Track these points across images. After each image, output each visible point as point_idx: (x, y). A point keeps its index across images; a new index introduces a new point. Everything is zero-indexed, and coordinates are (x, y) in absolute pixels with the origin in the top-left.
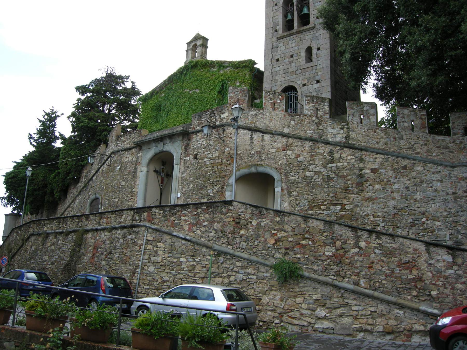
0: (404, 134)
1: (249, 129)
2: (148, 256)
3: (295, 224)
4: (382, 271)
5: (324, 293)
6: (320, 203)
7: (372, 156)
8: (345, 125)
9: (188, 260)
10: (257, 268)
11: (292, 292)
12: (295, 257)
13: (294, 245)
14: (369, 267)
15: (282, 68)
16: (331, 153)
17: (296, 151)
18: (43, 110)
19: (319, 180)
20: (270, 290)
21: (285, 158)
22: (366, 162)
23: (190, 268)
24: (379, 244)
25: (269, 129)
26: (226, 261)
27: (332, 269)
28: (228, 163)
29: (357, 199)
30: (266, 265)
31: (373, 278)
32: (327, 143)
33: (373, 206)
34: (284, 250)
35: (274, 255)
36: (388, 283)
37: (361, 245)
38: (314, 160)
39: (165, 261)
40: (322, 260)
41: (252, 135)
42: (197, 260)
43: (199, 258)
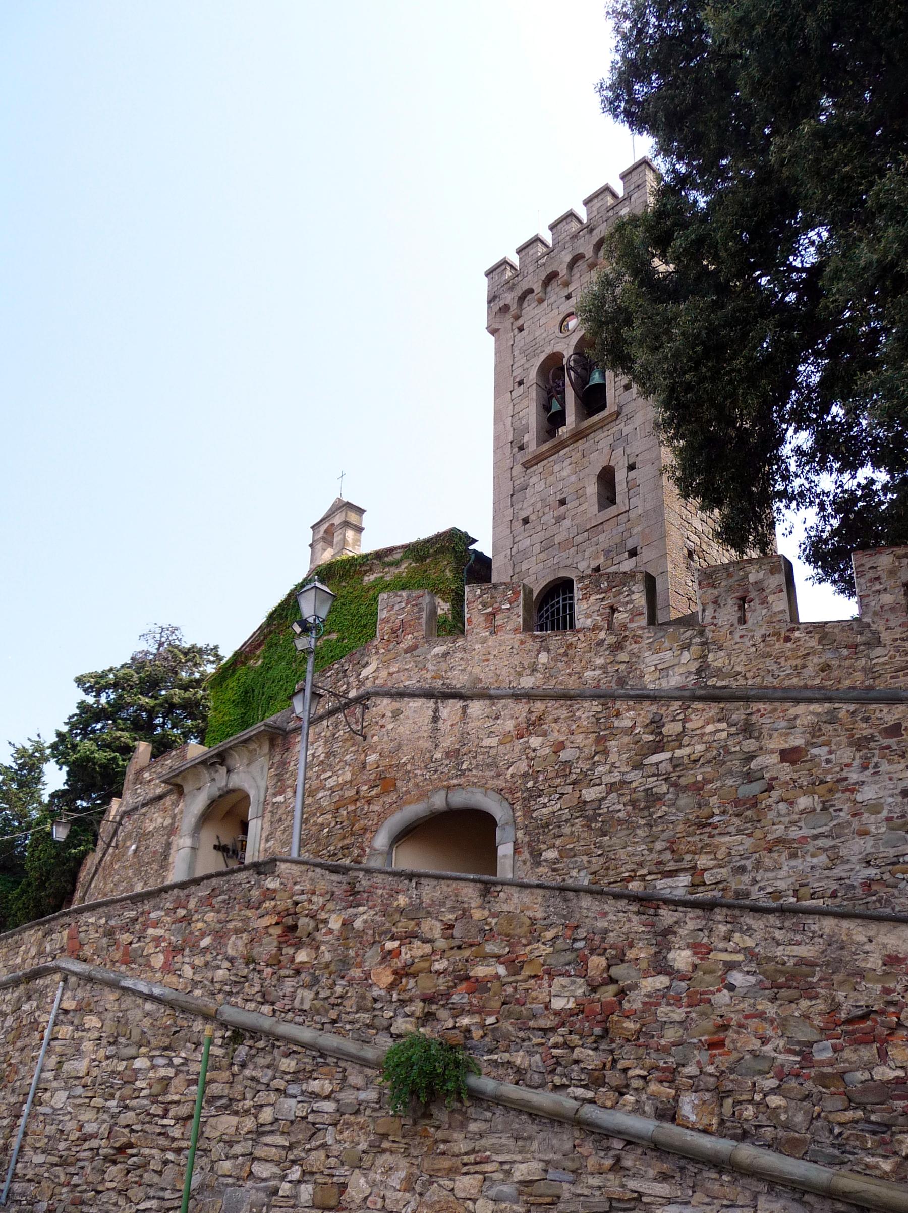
0: (882, 629)
1: (429, 695)
2: (58, 1059)
3: (453, 909)
4: (764, 1057)
5: (551, 1156)
6: (627, 874)
7: (783, 711)
8: (694, 637)
9: (155, 1062)
10: (340, 1076)
11: (443, 1154)
12: (454, 1028)
13: (451, 984)
14: (712, 1045)
15: (537, 538)
16: (656, 724)
17: (556, 734)
18: (10, 743)
19: (621, 807)
20: (377, 1149)
21: (524, 757)
22: (765, 732)
23: (157, 1089)
24: (746, 950)
25: (480, 685)
26: (254, 1056)
27: (577, 1062)
28: (373, 793)
29: (740, 848)
30: (364, 1063)
31: (730, 1086)
32: (643, 698)
33: (793, 863)
34: (421, 1004)
35: (391, 1025)
36: (793, 1104)
37: (675, 960)
38: (606, 752)
39: (95, 1072)
40: (545, 1031)
41: (436, 711)
42: (177, 1061)
43: (183, 1055)
